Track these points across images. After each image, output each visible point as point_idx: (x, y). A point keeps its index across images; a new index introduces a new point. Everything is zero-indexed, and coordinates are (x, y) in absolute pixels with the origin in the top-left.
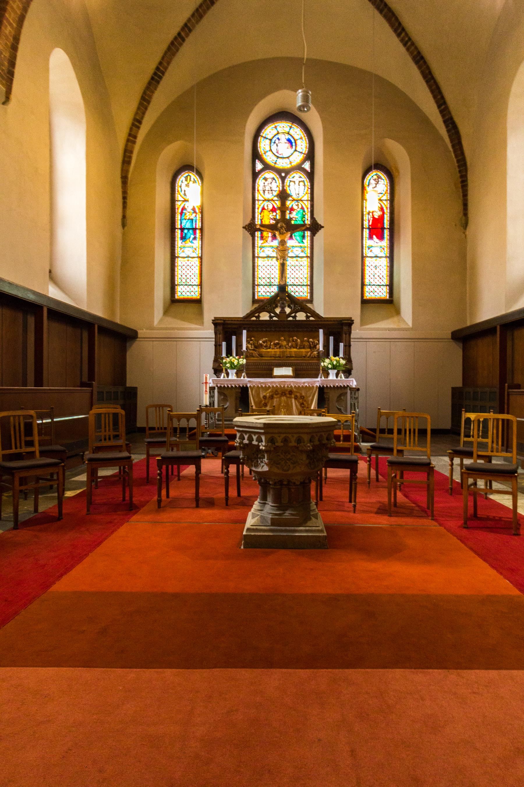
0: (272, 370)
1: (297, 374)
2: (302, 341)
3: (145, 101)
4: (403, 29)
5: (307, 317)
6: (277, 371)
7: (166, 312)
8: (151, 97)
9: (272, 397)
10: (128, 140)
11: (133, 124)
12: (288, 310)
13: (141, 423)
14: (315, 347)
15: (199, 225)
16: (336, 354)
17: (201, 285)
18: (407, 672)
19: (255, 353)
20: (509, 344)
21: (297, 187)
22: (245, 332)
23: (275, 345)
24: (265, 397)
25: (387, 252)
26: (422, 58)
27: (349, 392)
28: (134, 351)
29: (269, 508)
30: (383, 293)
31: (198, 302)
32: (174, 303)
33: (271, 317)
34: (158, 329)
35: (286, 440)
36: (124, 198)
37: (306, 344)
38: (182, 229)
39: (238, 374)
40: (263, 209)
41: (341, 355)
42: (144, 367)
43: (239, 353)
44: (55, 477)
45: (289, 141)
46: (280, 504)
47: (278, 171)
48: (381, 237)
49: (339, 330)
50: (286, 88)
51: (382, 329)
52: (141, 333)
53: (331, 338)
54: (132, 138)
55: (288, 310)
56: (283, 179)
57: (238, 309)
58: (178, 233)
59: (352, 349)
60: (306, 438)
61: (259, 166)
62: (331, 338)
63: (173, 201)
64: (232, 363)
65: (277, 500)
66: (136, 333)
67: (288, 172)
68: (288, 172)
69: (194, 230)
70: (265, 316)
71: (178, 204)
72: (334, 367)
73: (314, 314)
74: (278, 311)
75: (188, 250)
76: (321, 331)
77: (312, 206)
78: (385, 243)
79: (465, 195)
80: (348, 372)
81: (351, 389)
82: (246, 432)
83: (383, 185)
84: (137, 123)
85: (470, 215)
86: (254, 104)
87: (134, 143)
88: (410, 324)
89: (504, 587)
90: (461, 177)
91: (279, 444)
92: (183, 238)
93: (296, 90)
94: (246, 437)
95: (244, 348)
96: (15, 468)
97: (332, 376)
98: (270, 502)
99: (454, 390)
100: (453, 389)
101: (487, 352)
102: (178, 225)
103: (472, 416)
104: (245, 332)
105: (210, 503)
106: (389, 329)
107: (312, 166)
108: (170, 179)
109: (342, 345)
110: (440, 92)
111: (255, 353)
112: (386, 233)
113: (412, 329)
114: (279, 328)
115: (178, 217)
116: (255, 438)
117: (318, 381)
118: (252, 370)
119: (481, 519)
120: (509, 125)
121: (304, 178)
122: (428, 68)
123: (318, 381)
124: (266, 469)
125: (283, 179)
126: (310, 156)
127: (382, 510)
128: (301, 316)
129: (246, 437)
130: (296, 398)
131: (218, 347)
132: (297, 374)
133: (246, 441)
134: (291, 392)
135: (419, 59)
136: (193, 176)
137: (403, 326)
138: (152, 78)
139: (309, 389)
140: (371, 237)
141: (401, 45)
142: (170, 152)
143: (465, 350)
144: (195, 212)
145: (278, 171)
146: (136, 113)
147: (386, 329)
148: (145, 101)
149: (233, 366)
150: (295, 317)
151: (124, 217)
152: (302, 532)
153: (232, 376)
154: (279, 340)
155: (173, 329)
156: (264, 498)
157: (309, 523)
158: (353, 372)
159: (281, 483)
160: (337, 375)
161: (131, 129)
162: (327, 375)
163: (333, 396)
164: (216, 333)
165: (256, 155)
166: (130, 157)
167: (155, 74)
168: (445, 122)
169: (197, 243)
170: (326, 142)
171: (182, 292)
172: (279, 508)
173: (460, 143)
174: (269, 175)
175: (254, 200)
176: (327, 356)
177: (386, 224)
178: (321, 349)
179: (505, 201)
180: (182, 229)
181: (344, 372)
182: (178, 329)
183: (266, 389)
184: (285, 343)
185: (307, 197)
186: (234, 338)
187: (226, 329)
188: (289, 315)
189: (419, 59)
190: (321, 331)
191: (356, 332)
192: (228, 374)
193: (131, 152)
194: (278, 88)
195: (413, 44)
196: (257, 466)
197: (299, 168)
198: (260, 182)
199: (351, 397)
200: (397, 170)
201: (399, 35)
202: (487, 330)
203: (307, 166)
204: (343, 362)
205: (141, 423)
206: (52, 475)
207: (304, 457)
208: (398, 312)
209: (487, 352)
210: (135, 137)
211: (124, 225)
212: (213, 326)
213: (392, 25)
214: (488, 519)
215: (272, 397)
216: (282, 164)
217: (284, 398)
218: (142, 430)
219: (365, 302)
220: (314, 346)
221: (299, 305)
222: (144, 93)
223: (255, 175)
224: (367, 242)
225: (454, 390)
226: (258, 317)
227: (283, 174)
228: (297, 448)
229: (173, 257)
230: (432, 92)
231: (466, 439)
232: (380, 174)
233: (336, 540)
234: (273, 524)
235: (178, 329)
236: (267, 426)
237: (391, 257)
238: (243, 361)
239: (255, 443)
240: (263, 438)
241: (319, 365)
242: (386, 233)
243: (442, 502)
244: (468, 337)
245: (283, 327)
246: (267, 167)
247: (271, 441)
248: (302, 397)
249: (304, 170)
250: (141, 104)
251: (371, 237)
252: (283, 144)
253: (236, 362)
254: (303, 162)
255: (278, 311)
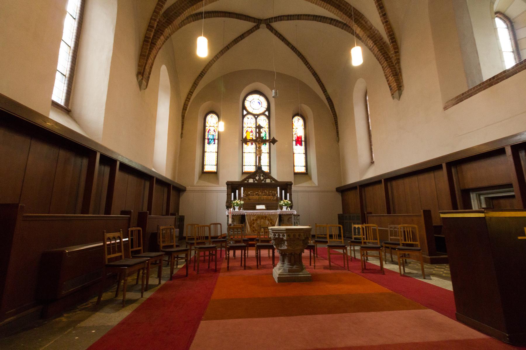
0: (255, 207)
1: (267, 208)
2: (269, 193)
3: (195, 84)
4: (308, 63)
5: (271, 181)
6: (258, 207)
7: (200, 178)
8: (198, 83)
9: (257, 220)
10: (186, 100)
11: (189, 94)
12: (262, 178)
13: (184, 235)
14: (275, 195)
15: (217, 138)
16: (286, 198)
17: (217, 165)
18: (363, 313)
19: (247, 198)
20: (363, 194)
21: (263, 121)
22: (242, 188)
23: (256, 194)
24: (253, 220)
25: (303, 151)
26: (316, 74)
27: (293, 217)
28: (184, 197)
29: (286, 265)
30: (303, 170)
31: (215, 173)
32: (204, 173)
33: (254, 181)
34: (196, 186)
35: (294, 235)
36: (183, 125)
37: (271, 194)
38: (208, 139)
39: (239, 209)
40: (247, 131)
41: (288, 198)
42: (188, 206)
43: (240, 198)
44: (158, 262)
45: (259, 103)
46: (291, 263)
47: (254, 115)
48: (301, 145)
49: (286, 187)
50: (258, 81)
51: (304, 187)
52: (188, 188)
53: (283, 191)
54: (188, 99)
55: (262, 178)
56: (256, 119)
57: (237, 178)
58: (206, 141)
59: (292, 196)
60: (302, 234)
61: (245, 113)
62: (283, 191)
63: (205, 126)
64: (237, 203)
65: (290, 261)
66: (186, 188)
67: (258, 115)
68: (258, 115)
69: (214, 140)
70: (251, 181)
71: (207, 128)
72: (286, 205)
73: (274, 180)
74: (257, 178)
75: (211, 150)
76: (278, 188)
77: (269, 131)
78: (303, 147)
79: (337, 128)
80: (291, 207)
81: (294, 215)
82: (277, 233)
83: (301, 122)
84: (191, 93)
85: (340, 136)
86: (244, 87)
87: (189, 101)
88: (317, 184)
89: (385, 290)
90: (335, 121)
91: (292, 237)
92: (209, 143)
93: (272, 90)
94: (277, 235)
95: (242, 196)
96: (173, 252)
97: (284, 209)
98: (286, 262)
99: (339, 216)
100: (338, 215)
101: (353, 198)
102: (206, 137)
103: (357, 226)
104: (242, 188)
105: (250, 268)
106: (308, 187)
107: (269, 113)
108: (204, 116)
109: (288, 194)
110: (324, 87)
111: (247, 198)
112: (303, 143)
113: (318, 187)
114: (257, 186)
115: (207, 133)
116: (281, 235)
117: (279, 211)
118: (246, 207)
119: (367, 270)
120: (354, 102)
121: (265, 118)
122: (319, 77)
123: (279, 211)
124: (286, 248)
125: (256, 119)
126: (268, 109)
127: (325, 268)
128: (268, 181)
129: (277, 235)
130: (268, 220)
131: (229, 196)
132: (267, 208)
133: (277, 237)
134: (266, 217)
135: (315, 74)
136: (214, 116)
137: (313, 185)
138: (200, 76)
139: (274, 215)
140: (296, 145)
141: (307, 69)
142: (205, 105)
143: (342, 196)
144: (215, 131)
145: (254, 115)
146: (191, 89)
147: (306, 187)
148: (195, 84)
149: (237, 205)
150: (265, 181)
151: (182, 133)
152: (301, 275)
153: (237, 210)
154: (258, 192)
155: (204, 186)
156: (283, 261)
157: (303, 271)
158: (293, 207)
159: (291, 254)
160: (287, 208)
161: (188, 96)
162: (282, 209)
163: (285, 219)
164: (227, 189)
165: (244, 108)
166: (187, 107)
167: (201, 74)
168: (327, 99)
169: (216, 145)
170: (276, 105)
171: (207, 169)
172: (291, 265)
173: (333, 107)
174: (250, 116)
175: (243, 127)
176: (282, 199)
177: (303, 139)
178: (279, 196)
179: (355, 130)
180: (208, 139)
181: (290, 207)
182: (207, 186)
183: (254, 215)
184: (261, 193)
185: (267, 126)
186: (237, 191)
187: (232, 187)
188: (263, 180)
189: (315, 74)
190: (278, 188)
191: (294, 188)
192: (234, 209)
193: (187, 105)
194: (254, 81)
195: (312, 69)
196: (281, 247)
197: (263, 114)
198: (245, 119)
199: (295, 219)
200: (307, 117)
201: (306, 65)
202: (353, 187)
203: (267, 113)
204: (290, 202)
205: (184, 235)
206: (156, 261)
207: (301, 242)
208: (310, 179)
209: (353, 198)
210: (190, 99)
211: (181, 137)
212: (226, 185)
213: (303, 61)
214: (370, 269)
215: (257, 220)
216: (255, 112)
217: (262, 220)
218: (185, 238)
219: (296, 174)
220: (274, 195)
221: (267, 175)
222: (195, 81)
223: (243, 116)
224: (295, 147)
225: (339, 216)
226: (248, 181)
227: (256, 116)
228: (298, 238)
229: (204, 152)
230: (321, 87)
231: (355, 236)
232: (299, 118)
233: (313, 279)
234: (289, 272)
235: (207, 186)
236: (287, 229)
237: (306, 154)
238: (242, 202)
239: (281, 237)
240: (285, 235)
241: (278, 204)
242: (303, 143)
243: (351, 264)
244: (344, 190)
245: (260, 186)
246: (249, 113)
247: (288, 236)
248: (271, 219)
249: (265, 115)
250: (193, 85)
251: (296, 145)
252: (256, 103)
253: (239, 203)
254: (265, 111)
255: (257, 178)
